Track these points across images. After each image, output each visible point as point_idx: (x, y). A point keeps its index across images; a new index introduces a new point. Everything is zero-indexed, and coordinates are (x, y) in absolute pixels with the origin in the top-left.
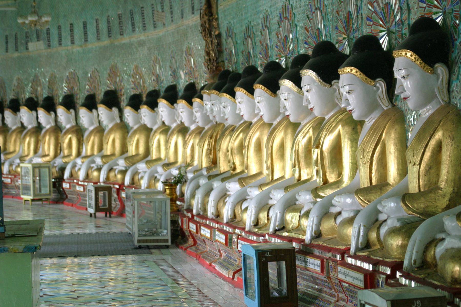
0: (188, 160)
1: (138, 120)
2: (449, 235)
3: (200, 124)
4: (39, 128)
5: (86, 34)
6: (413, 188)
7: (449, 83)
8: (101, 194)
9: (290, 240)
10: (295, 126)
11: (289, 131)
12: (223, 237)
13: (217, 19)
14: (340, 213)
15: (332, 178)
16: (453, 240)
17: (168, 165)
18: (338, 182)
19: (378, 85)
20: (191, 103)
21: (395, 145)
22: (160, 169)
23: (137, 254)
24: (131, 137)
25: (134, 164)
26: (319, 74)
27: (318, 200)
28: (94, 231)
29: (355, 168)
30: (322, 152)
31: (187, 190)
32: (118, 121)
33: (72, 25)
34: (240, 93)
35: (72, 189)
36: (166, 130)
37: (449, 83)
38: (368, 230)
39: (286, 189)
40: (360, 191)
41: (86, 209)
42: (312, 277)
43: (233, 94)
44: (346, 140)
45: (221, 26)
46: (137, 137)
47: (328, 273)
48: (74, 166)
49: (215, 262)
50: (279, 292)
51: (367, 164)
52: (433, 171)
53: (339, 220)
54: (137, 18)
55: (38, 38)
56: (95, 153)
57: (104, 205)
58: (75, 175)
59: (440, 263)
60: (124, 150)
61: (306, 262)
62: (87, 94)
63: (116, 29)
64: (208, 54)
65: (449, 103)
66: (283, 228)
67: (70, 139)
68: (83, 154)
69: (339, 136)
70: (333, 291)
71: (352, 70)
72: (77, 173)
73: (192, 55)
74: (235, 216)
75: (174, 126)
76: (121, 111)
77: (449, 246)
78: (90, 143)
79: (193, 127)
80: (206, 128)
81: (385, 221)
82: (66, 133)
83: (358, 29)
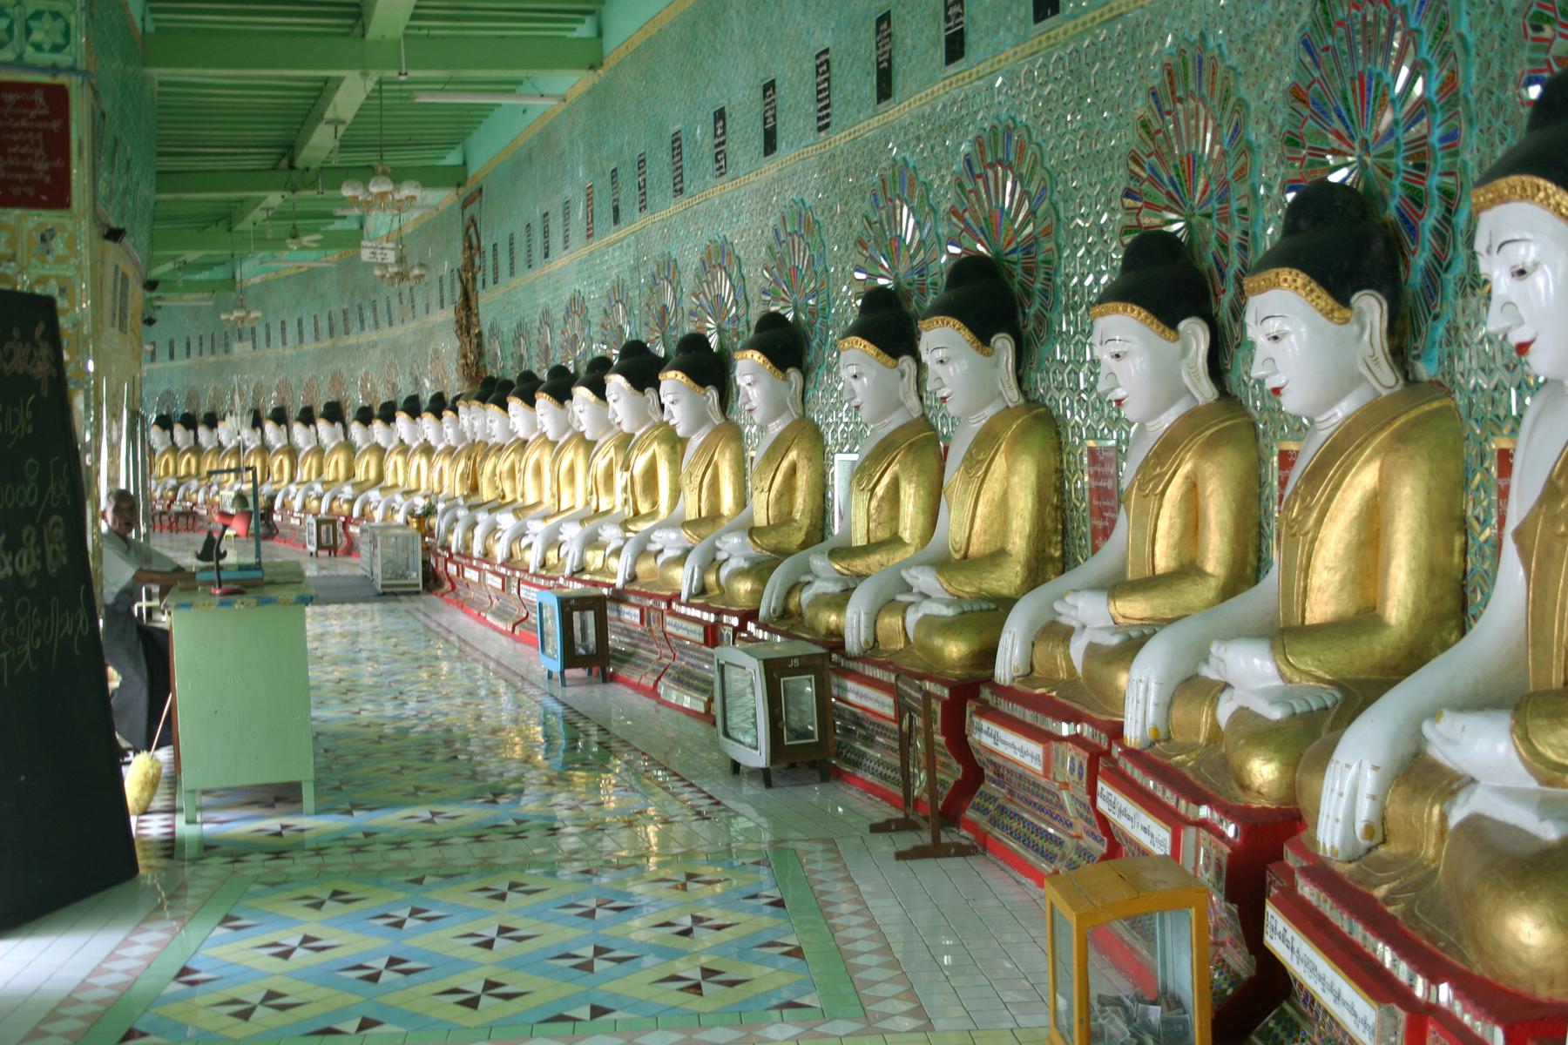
0: (436, 489)
1: (367, 439)
2: (817, 577)
3: (452, 443)
5: (301, 333)
6: (760, 519)
8: (324, 528)
9: (595, 584)
10: (589, 445)
11: (581, 451)
12: (499, 580)
13: (477, 315)
14: (661, 551)
15: (644, 508)
16: (825, 584)
17: (408, 493)
18: (653, 514)
20: (439, 417)
21: (731, 467)
22: (398, 498)
23: (381, 601)
24: (359, 459)
25: (363, 492)
26: (629, 379)
27: (628, 535)
28: (315, 574)
29: (676, 492)
30: (632, 476)
31: (434, 521)
32: (342, 439)
33: (283, 323)
34: (515, 404)
35: (285, 522)
36: (404, 449)
38: (704, 571)
39: (582, 522)
40: (686, 524)
41: (305, 546)
42: (627, 630)
43: (504, 406)
45: (483, 322)
46: (367, 457)
47: (649, 624)
48: (287, 494)
49: (485, 611)
50: (586, 648)
52: (785, 499)
53: (661, 559)
54: (368, 313)
55: (240, 338)
56: (313, 478)
57: (328, 541)
58: (287, 505)
59: (808, 613)
60: (350, 474)
61: (619, 611)
62: (301, 406)
63: (340, 324)
64: (465, 356)
66: (582, 570)
67: (281, 461)
68: (298, 478)
69: (654, 456)
70: (654, 647)
72: (290, 502)
74: (511, 555)
76: (346, 428)
77: (820, 591)
78: (1174, 491)
79: (441, 447)
80: (460, 447)
81: (726, 560)
82: (275, 454)
83: (676, 326)
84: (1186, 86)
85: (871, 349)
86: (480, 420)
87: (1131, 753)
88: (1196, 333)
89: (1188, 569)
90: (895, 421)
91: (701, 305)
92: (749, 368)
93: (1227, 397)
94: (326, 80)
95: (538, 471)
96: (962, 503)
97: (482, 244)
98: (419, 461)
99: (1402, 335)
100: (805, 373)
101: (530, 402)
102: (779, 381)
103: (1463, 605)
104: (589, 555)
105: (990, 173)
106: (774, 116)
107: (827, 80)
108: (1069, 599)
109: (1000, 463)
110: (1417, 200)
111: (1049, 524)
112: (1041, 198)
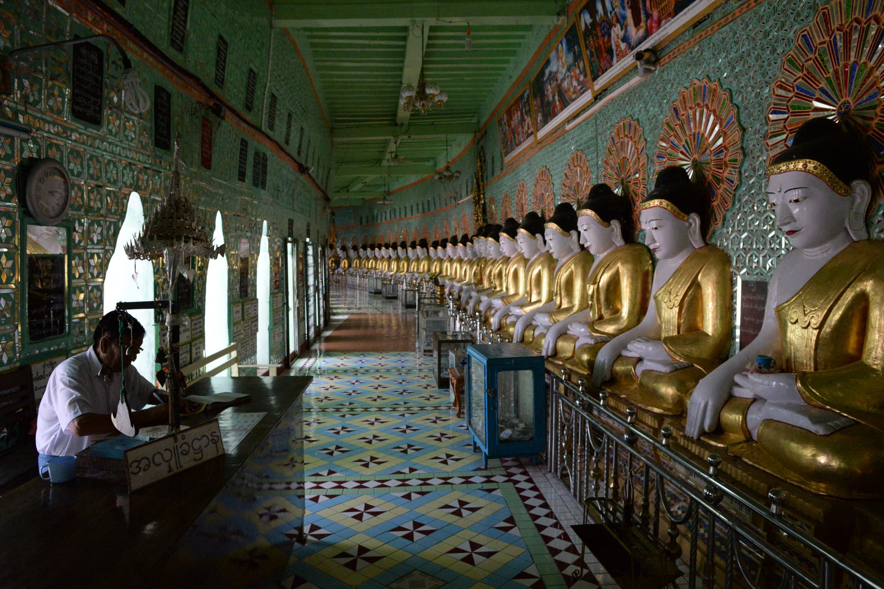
1: (436, 254)
3: (471, 258)
4: (390, 257)
17: (451, 279)
19: (691, 220)
20: (465, 245)
22: (447, 282)
43: (497, 239)
44: (626, 278)
51: (674, 308)
71: (661, 203)
73: (287, 509)
75: (455, 258)
86: (486, 245)
92: (552, 228)
94: (387, 140)
98: (456, 265)
101: (380, 249)
104: (560, 344)
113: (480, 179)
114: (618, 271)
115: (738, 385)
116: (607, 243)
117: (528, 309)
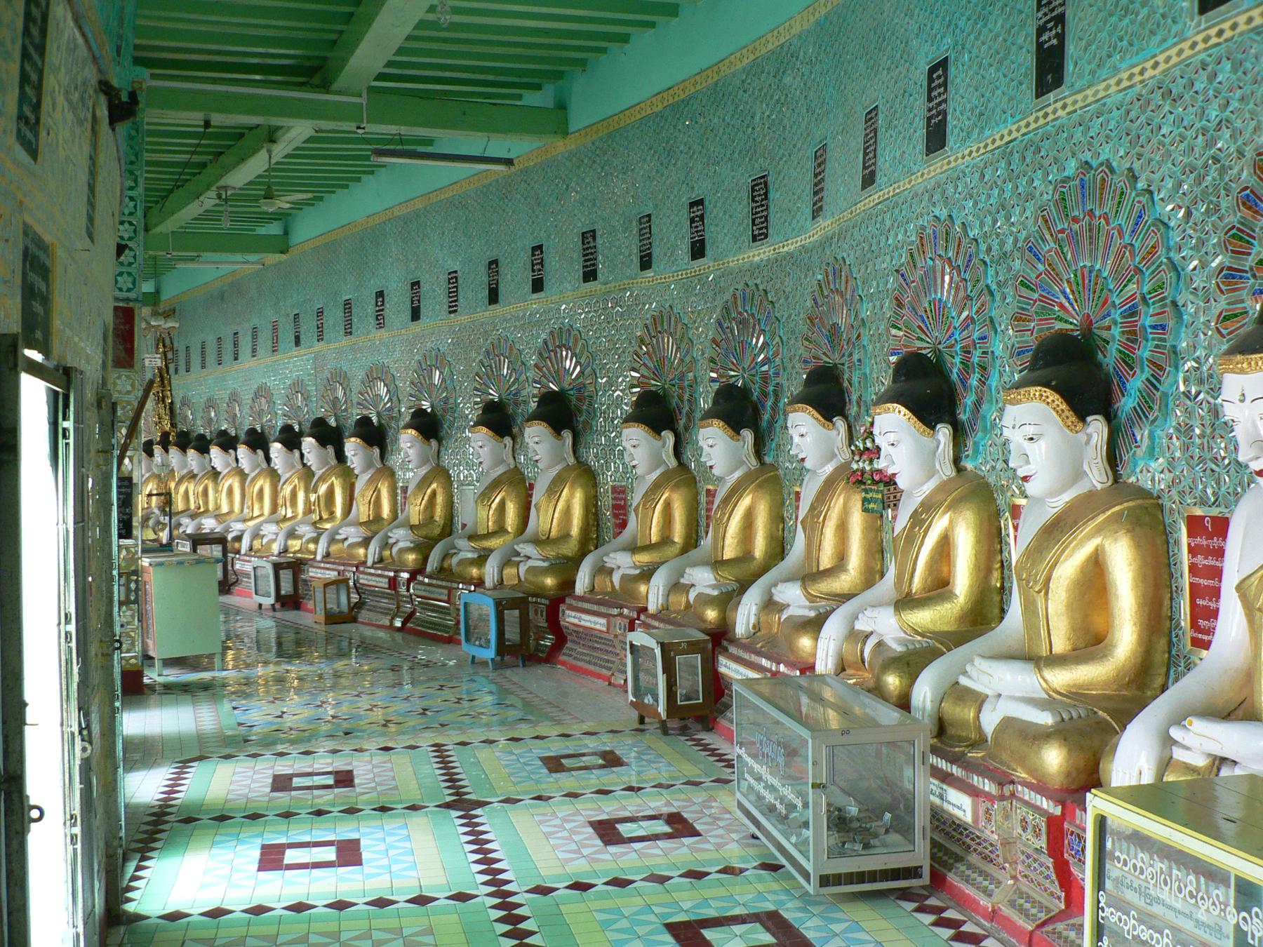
7: (439, 452)
14: (346, 539)
37: (439, 452)
40: (361, 524)
53: (346, 544)
65: (438, 465)
84: (663, 326)
85: (491, 433)
87: (653, 617)
88: (668, 436)
89: (666, 540)
90: (500, 470)
91: (365, 400)
92: (407, 442)
93: (682, 465)
95: (230, 491)
96: (547, 511)
97: (176, 345)
99: (759, 446)
100: (440, 441)
102: (426, 447)
103: (783, 552)
104: (290, 542)
105: (558, 350)
106: (419, 301)
107: (456, 287)
108: (611, 555)
109: (566, 491)
110: (765, 394)
111: (591, 523)
112: (588, 365)
113: (165, 371)
114: (332, 484)
115: (1175, 742)
116: (324, 462)
117: (251, 523)
